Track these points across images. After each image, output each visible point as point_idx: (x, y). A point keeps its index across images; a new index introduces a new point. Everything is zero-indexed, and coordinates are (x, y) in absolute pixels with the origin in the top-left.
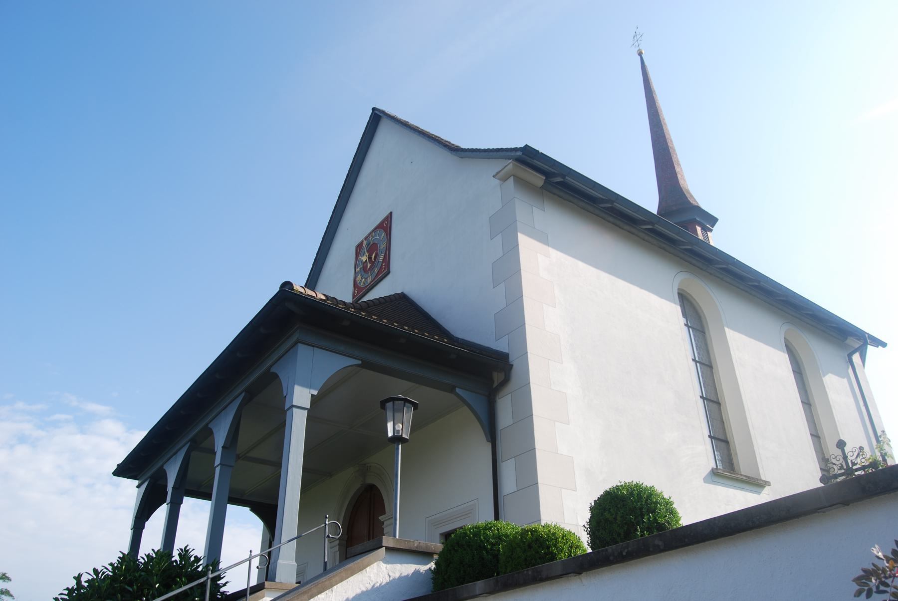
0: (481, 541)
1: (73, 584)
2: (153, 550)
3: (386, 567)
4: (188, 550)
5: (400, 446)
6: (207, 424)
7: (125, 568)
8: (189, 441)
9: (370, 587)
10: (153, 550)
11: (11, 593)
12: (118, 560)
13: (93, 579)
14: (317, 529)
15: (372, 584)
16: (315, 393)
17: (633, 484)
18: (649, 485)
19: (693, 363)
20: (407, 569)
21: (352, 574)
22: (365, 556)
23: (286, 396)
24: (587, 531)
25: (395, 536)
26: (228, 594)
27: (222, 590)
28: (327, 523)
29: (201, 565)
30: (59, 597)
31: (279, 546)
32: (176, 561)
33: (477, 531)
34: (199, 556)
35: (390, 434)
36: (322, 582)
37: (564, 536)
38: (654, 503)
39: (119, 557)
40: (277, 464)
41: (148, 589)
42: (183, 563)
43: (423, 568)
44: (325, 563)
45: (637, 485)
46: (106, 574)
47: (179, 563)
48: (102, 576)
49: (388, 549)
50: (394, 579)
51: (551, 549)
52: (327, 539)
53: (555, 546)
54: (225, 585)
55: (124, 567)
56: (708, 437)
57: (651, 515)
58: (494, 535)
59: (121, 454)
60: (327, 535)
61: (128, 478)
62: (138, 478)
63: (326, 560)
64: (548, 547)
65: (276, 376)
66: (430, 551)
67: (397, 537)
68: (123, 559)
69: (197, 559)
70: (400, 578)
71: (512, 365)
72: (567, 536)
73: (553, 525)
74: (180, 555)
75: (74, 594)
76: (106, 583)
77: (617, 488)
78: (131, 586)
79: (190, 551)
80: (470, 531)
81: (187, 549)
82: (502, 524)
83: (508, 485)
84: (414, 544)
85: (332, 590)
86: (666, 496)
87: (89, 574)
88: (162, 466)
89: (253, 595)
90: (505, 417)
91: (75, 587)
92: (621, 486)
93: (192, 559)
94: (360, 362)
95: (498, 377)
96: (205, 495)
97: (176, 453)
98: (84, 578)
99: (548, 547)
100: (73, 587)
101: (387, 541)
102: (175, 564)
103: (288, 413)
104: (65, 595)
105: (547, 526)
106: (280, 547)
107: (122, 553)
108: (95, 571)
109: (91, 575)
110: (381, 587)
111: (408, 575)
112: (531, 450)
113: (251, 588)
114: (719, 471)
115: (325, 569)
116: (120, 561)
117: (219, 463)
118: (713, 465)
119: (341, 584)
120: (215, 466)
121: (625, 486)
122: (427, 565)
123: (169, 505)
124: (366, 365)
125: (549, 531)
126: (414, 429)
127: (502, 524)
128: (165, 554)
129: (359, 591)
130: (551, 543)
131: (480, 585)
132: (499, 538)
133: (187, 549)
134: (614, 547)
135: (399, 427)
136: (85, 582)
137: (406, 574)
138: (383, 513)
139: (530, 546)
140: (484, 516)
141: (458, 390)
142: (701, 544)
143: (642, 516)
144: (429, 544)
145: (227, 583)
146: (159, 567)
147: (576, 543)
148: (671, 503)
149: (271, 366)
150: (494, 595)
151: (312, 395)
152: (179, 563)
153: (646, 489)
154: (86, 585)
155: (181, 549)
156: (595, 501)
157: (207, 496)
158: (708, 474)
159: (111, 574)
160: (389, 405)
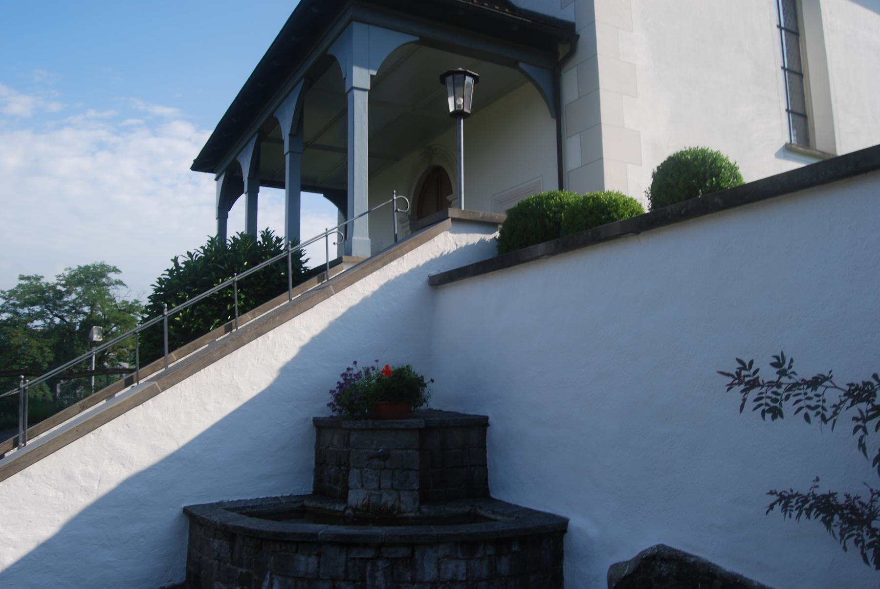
0: (543, 209)
1: (171, 265)
2: (237, 233)
3: (453, 237)
4: (269, 232)
5: (462, 121)
6: (272, 114)
7: (215, 249)
8: (256, 133)
9: (438, 255)
10: (237, 233)
11: (125, 282)
12: (208, 244)
13: (188, 261)
14: (385, 205)
15: (440, 253)
16: (374, 73)
17: (698, 149)
18: (715, 150)
19: (778, 30)
20: (473, 238)
21: (421, 244)
22: (431, 227)
23: (345, 79)
24: (648, 196)
25: (460, 207)
26: (310, 269)
27: (304, 265)
28: (395, 198)
29: (283, 244)
30: (162, 277)
31: (353, 219)
32: (259, 242)
33: (540, 201)
34: (280, 237)
35: (451, 109)
36: (394, 251)
37: (625, 202)
38: (718, 168)
39: (208, 241)
40: (343, 150)
41: (238, 267)
42: (266, 243)
43: (488, 237)
44: (396, 236)
45: (703, 151)
46: (199, 256)
47: (262, 243)
48: (196, 258)
49: (454, 220)
50: (461, 248)
51: (611, 215)
52: (395, 214)
53: (616, 211)
54: (306, 261)
55: (213, 249)
56: (776, 27)
57: (714, 179)
58: (556, 203)
59: (195, 153)
60: (395, 209)
61: (206, 172)
62: (215, 171)
63: (396, 232)
64: (609, 213)
65: (332, 60)
66: (494, 221)
67: (463, 209)
68: (212, 241)
69: (279, 240)
70: (467, 247)
71: (578, 37)
72: (628, 203)
73: (615, 192)
74: (262, 236)
75: (174, 274)
76: (201, 262)
77: (682, 153)
78: (223, 264)
79: (271, 232)
80: (533, 201)
81: (268, 231)
82: (565, 194)
83: (573, 160)
84: (479, 215)
85: (403, 258)
86: (732, 161)
87: (184, 257)
88: (235, 158)
89: (333, 269)
90: (570, 92)
91: (174, 268)
92: (686, 151)
93: (274, 239)
94: (417, 39)
95: (563, 49)
96: (278, 184)
97: (246, 145)
98: (180, 261)
99: (609, 213)
100: (172, 269)
101: (452, 212)
102: (259, 244)
103: (349, 95)
104: (166, 275)
105: (609, 193)
106: (353, 221)
107: (211, 237)
108: (189, 254)
109: (186, 258)
110: (449, 255)
111: (474, 244)
112: (597, 125)
113: (330, 262)
114: (793, 146)
115: (396, 240)
116: (210, 244)
117: (286, 156)
118: (787, 140)
119: (411, 252)
120: (285, 154)
121: (690, 151)
122: (491, 233)
123: (247, 194)
124: (423, 41)
125: (611, 198)
126: (474, 108)
127: (565, 194)
128: (249, 236)
129: (428, 259)
130: (612, 209)
131: (541, 247)
132: (561, 206)
133: (268, 231)
134: (673, 206)
135: (461, 101)
136: (182, 263)
137: (472, 243)
138: (451, 193)
139: (591, 212)
140: (549, 186)
141: (521, 65)
142: (761, 202)
143: (705, 180)
144: (493, 214)
145: (308, 259)
146: (244, 247)
147: (637, 209)
148: (737, 169)
149: (327, 49)
150: (554, 257)
151: (372, 76)
152: (262, 243)
153: (711, 154)
154: (183, 266)
155: (263, 232)
156: (658, 168)
157: (280, 185)
158: (781, 149)
159: (203, 255)
160: (449, 79)
